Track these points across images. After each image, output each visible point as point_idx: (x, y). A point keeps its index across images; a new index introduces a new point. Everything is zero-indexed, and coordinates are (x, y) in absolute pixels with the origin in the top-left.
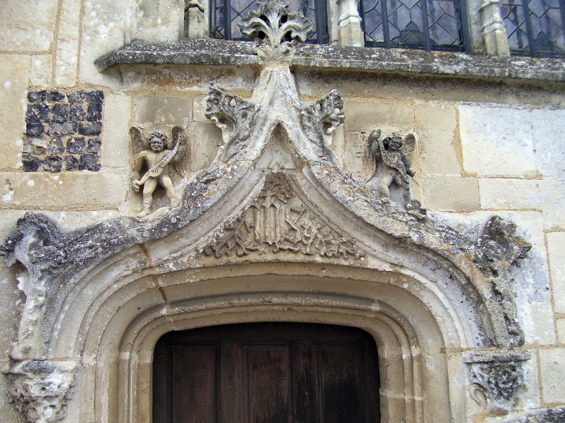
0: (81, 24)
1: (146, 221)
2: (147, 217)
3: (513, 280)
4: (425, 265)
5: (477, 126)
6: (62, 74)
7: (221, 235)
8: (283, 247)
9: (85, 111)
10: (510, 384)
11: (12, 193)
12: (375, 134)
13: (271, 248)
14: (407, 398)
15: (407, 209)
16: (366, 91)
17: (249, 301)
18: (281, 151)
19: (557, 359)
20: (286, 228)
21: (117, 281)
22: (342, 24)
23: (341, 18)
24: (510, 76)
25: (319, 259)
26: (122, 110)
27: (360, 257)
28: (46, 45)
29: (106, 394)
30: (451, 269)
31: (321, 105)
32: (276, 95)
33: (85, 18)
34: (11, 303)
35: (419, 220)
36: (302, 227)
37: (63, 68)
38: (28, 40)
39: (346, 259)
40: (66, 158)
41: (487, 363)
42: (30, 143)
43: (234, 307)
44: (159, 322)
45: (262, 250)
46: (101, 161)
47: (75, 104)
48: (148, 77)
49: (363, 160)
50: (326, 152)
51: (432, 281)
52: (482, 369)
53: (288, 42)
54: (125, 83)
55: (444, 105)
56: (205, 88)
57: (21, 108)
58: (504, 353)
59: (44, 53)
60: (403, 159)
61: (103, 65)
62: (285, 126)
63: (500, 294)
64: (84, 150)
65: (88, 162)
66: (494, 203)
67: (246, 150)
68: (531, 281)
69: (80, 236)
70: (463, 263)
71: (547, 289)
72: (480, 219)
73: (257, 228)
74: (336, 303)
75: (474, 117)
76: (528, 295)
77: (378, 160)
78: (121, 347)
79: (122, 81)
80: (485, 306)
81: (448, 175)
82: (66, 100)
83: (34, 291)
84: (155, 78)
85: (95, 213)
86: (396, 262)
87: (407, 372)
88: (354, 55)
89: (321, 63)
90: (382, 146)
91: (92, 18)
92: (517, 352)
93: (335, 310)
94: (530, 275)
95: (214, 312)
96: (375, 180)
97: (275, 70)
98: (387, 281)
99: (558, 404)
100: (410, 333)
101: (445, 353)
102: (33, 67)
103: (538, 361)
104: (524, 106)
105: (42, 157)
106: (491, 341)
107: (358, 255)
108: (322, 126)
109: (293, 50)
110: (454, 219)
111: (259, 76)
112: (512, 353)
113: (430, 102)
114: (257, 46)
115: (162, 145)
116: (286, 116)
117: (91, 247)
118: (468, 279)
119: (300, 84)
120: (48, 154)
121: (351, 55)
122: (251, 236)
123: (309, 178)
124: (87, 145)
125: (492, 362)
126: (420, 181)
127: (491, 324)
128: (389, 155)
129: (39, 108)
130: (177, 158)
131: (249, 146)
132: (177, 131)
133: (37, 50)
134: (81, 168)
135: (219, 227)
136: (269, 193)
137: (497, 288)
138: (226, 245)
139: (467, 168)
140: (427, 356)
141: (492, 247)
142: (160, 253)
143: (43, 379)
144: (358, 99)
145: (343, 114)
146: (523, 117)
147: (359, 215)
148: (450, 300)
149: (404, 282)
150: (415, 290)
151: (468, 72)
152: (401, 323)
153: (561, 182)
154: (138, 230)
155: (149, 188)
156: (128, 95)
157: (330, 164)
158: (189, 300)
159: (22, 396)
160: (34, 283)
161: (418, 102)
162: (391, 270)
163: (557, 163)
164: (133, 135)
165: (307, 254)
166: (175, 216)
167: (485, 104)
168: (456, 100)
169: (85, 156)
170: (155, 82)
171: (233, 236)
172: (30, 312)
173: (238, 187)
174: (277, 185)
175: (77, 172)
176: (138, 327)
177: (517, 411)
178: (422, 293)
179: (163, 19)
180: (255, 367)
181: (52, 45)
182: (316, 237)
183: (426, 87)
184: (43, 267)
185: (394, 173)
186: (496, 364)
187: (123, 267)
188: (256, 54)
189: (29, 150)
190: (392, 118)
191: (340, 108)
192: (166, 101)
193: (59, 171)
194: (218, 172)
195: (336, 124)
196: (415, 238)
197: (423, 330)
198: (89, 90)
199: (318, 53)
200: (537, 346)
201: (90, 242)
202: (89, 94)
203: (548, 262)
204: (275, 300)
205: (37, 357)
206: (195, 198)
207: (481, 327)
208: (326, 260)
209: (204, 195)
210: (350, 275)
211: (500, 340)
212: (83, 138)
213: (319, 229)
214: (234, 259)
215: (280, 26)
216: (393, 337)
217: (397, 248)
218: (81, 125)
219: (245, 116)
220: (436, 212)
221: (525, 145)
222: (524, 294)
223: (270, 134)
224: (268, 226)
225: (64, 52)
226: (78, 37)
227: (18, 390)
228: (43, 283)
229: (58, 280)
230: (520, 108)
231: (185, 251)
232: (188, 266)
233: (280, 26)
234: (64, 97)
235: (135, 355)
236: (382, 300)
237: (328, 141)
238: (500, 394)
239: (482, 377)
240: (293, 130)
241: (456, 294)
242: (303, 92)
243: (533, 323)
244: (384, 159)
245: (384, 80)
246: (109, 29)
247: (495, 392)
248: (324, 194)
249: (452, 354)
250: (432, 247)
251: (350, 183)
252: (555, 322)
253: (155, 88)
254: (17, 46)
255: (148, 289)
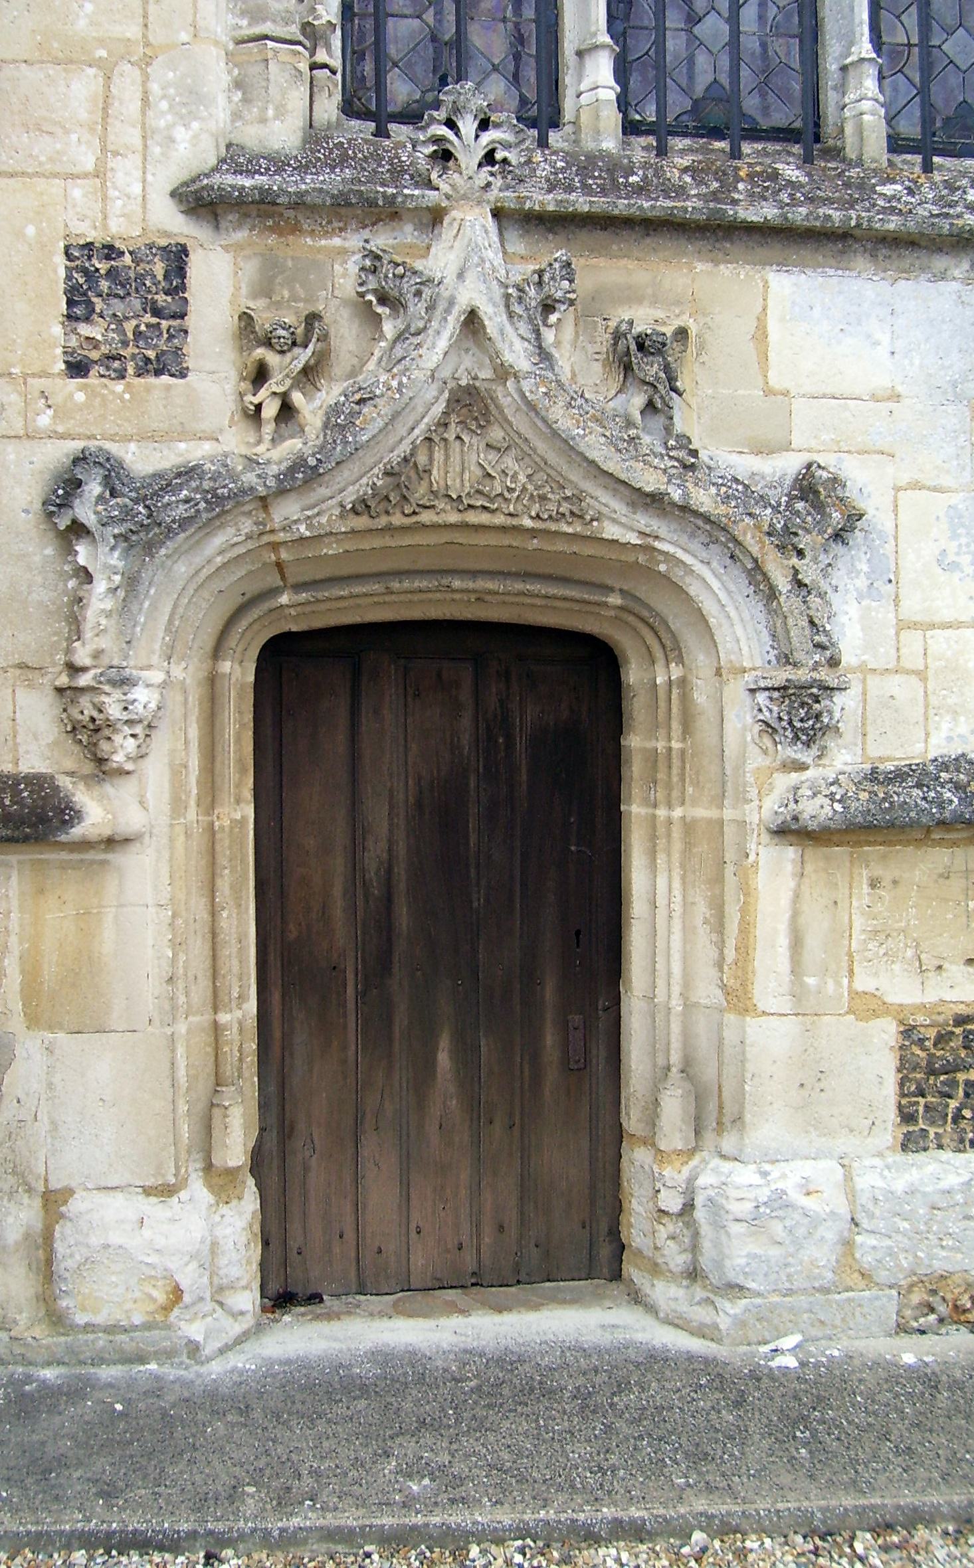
0: (144, 124)
1: (269, 462)
2: (268, 455)
3: (830, 565)
4: (692, 536)
5: (797, 309)
6: (118, 213)
7: (380, 483)
8: (472, 502)
9: (160, 277)
10: (811, 722)
11: (50, 412)
12: (624, 327)
13: (455, 504)
14: (661, 745)
15: (667, 448)
16: (615, 247)
17: (416, 584)
18: (474, 350)
19: (895, 691)
20: (479, 472)
21: (220, 553)
22: (584, 99)
23: (582, 87)
24: (858, 225)
25: (528, 523)
26: (220, 278)
27: (592, 520)
28: (88, 162)
29: (195, 725)
30: (730, 545)
31: (540, 277)
32: (469, 259)
33: (150, 113)
34: (61, 585)
35: (685, 467)
36: (503, 471)
37: (119, 203)
38: (58, 152)
39: (569, 524)
40: (134, 356)
41: (778, 689)
42: (74, 331)
43: (392, 593)
44: (274, 615)
45: (442, 506)
46: (190, 363)
47: (142, 265)
48: (260, 222)
49: (604, 366)
50: (544, 355)
51: (702, 562)
52: (771, 699)
53: (489, 168)
54: (222, 231)
55: (744, 272)
56: (353, 240)
57: (55, 271)
58: (802, 675)
59: (86, 176)
60: (667, 368)
61: (188, 202)
62: (481, 314)
63: (806, 585)
64: (162, 345)
65: (167, 365)
66: (811, 440)
67: (421, 352)
68: (865, 567)
69: (165, 483)
70: (749, 536)
71: (890, 581)
72: (789, 465)
73: (435, 472)
74: (553, 590)
75: (794, 293)
76: (857, 590)
77: (628, 368)
78: (217, 653)
79: (217, 228)
80: (779, 603)
81: (741, 392)
82: (127, 259)
83: (106, 566)
84: (271, 223)
85: (182, 446)
86: (648, 530)
87: (662, 704)
88: (600, 177)
89: (542, 203)
90: (633, 347)
91: (163, 113)
92: (824, 675)
93: (550, 603)
94: (864, 558)
95: (358, 601)
96: (622, 397)
97: (468, 218)
98: (633, 559)
99: (889, 759)
100: (668, 643)
101: (721, 676)
102: (69, 200)
103: (864, 693)
104: (882, 275)
105: (95, 355)
106: (786, 656)
107: (588, 518)
108: (540, 309)
109: (498, 182)
110: (744, 465)
111: (442, 223)
112: (815, 675)
113: (722, 267)
114: (440, 176)
115: (290, 342)
116: (484, 298)
117: (187, 501)
118: (756, 561)
119: (506, 235)
120: (105, 349)
121: (596, 178)
122: (425, 484)
123: (516, 396)
124: (166, 336)
125: (785, 688)
126: (693, 402)
127: (788, 632)
128: (646, 361)
129: (85, 271)
130: (312, 362)
131: (425, 347)
132: (312, 319)
133: (74, 172)
134: (158, 373)
135: (376, 471)
136: (454, 418)
137: (800, 577)
138: (387, 498)
139: (775, 381)
140: (695, 680)
141: (797, 514)
142: (288, 510)
143: (125, 694)
144: (602, 262)
145: (574, 291)
146: (878, 295)
147: (591, 457)
148: (729, 592)
149: (661, 562)
150: (677, 574)
151: (786, 218)
152: (655, 625)
153: (931, 408)
154: (259, 476)
155: (271, 410)
156: (228, 252)
157: (550, 375)
158: (322, 581)
159: (93, 720)
160: (105, 555)
161: (700, 267)
162: (639, 542)
163: (930, 375)
164: (243, 324)
165: (511, 515)
166: (314, 455)
167: (815, 271)
168: (765, 263)
169: (163, 353)
170: (272, 229)
171: (398, 485)
172: (100, 598)
173: (407, 410)
174: (466, 405)
175: (151, 380)
176: (244, 623)
177: (824, 766)
178: (688, 580)
179: (276, 109)
180: (417, 696)
181: (99, 163)
182: (524, 489)
183: (717, 241)
184: (116, 531)
185: (651, 390)
186: (791, 691)
187: (231, 531)
188: (438, 189)
189: (74, 342)
190: (654, 295)
191: (571, 281)
192: (290, 263)
193: (123, 377)
194: (378, 387)
195: (563, 307)
196: (676, 495)
197: (690, 639)
198: (163, 242)
199: (538, 173)
200: (865, 670)
201: (185, 492)
202: (164, 249)
203: (896, 538)
204: (457, 584)
205: (115, 662)
206: (342, 428)
207: (774, 636)
208: (538, 525)
209: (357, 423)
210: (575, 549)
211: (799, 656)
212: (159, 324)
213: (529, 476)
214: (397, 520)
215: (477, 137)
216: (644, 649)
217: (650, 509)
218: (154, 302)
219: (418, 293)
220: (718, 452)
221: (877, 343)
222: (850, 587)
223: (458, 327)
224: (451, 470)
225: (120, 175)
226: (140, 148)
227: (85, 712)
228: (116, 554)
229: (138, 549)
230: (874, 278)
231: (324, 506)
232: (328, 529)
233: (477, 137)
234: (123, 253)
235: (236, 666)
236: (625, 588)
237: (549, 336)
238: (797, 738)
239: (771, 711)
240: (493, 319)
241: (739, 583)
242: (510, 249)
243: (860, 634)
244: (635, 367)
245: (647, 228)
246: (191, 133)
247: (789, 733)
248: (539, 423)
249: (731, 676)
250: (702, 510)
251: (580, 407)
252: (897, 634)
253: (272, 240)
254: (41, 164)
255: (264, 564)
